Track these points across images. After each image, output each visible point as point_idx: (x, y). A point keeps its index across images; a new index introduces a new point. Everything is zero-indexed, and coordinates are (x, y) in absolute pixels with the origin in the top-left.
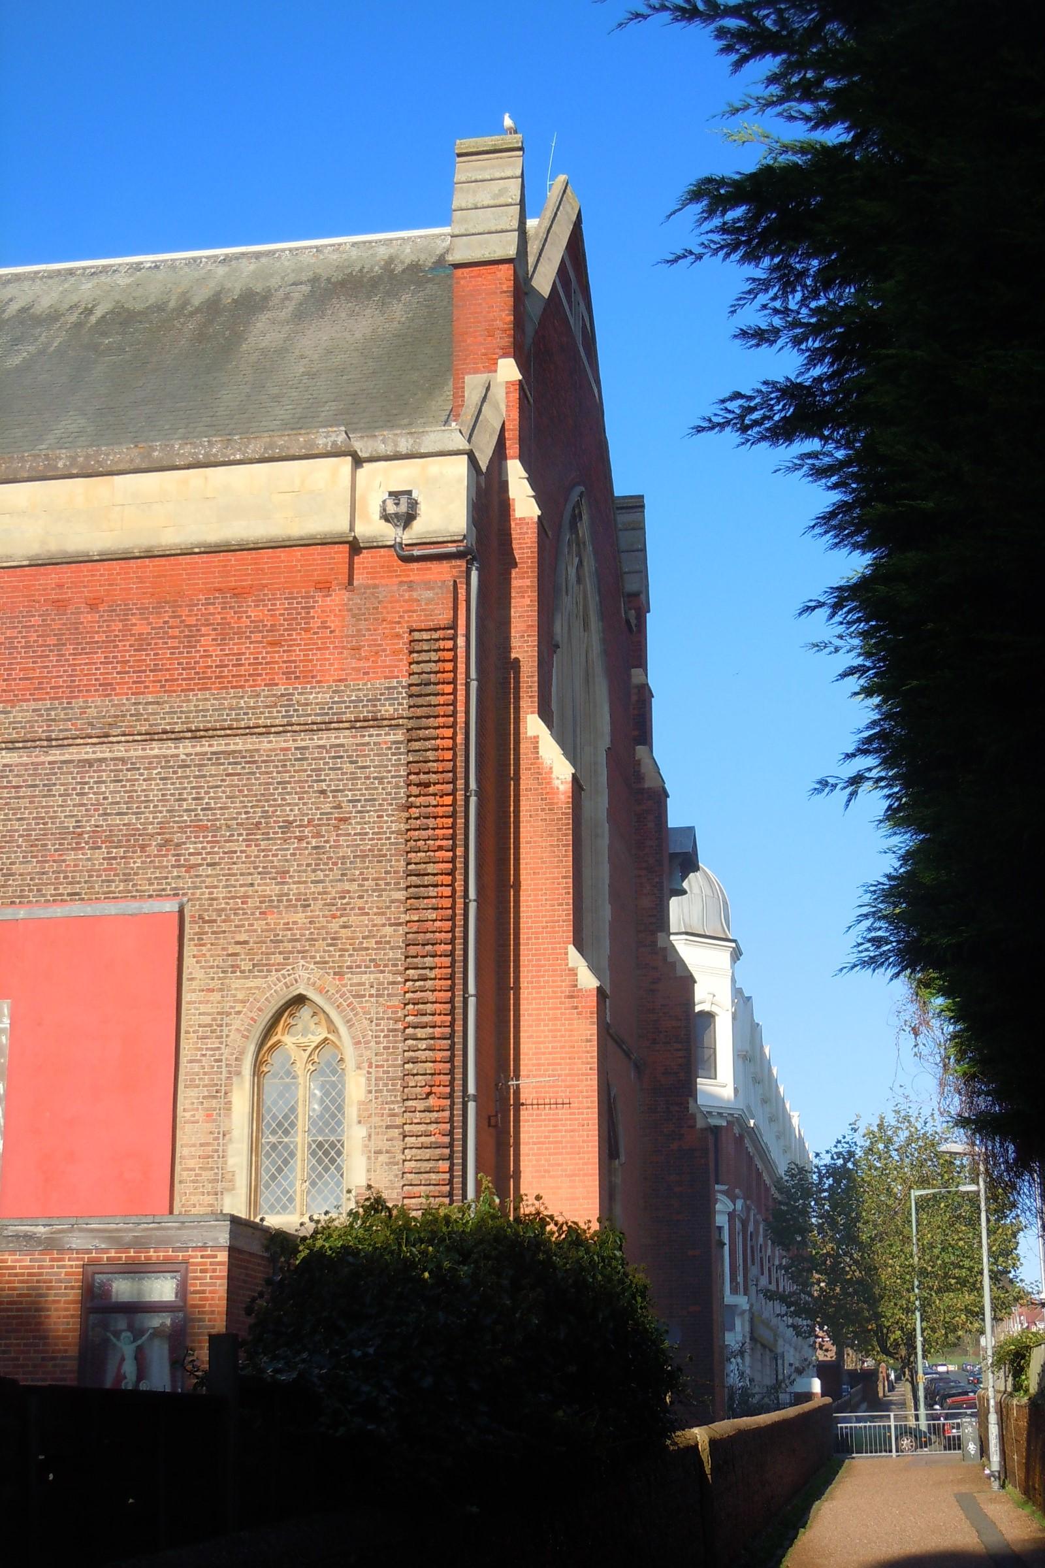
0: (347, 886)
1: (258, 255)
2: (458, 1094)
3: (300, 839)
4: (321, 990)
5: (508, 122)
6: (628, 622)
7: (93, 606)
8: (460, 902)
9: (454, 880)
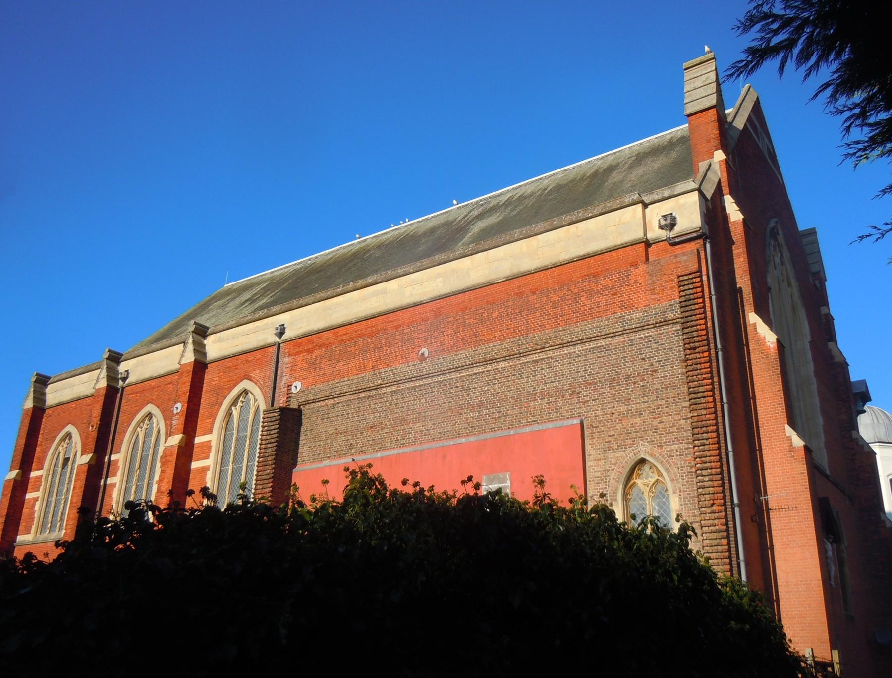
0: (660, 403)
1: (615, 153)
2: (729, 503)
3: (635, 383)
4: (652, 455)
5: (707, 48)
6: (815, 285)
7: (533, 293)
8: (718, 405)
9: (714, 394)
